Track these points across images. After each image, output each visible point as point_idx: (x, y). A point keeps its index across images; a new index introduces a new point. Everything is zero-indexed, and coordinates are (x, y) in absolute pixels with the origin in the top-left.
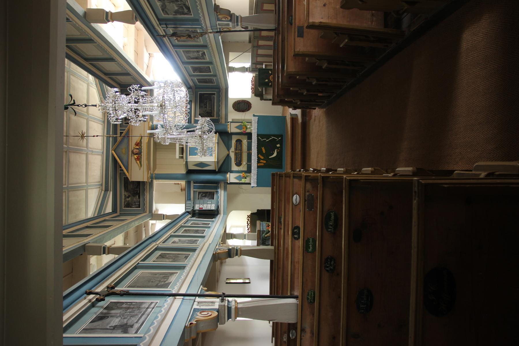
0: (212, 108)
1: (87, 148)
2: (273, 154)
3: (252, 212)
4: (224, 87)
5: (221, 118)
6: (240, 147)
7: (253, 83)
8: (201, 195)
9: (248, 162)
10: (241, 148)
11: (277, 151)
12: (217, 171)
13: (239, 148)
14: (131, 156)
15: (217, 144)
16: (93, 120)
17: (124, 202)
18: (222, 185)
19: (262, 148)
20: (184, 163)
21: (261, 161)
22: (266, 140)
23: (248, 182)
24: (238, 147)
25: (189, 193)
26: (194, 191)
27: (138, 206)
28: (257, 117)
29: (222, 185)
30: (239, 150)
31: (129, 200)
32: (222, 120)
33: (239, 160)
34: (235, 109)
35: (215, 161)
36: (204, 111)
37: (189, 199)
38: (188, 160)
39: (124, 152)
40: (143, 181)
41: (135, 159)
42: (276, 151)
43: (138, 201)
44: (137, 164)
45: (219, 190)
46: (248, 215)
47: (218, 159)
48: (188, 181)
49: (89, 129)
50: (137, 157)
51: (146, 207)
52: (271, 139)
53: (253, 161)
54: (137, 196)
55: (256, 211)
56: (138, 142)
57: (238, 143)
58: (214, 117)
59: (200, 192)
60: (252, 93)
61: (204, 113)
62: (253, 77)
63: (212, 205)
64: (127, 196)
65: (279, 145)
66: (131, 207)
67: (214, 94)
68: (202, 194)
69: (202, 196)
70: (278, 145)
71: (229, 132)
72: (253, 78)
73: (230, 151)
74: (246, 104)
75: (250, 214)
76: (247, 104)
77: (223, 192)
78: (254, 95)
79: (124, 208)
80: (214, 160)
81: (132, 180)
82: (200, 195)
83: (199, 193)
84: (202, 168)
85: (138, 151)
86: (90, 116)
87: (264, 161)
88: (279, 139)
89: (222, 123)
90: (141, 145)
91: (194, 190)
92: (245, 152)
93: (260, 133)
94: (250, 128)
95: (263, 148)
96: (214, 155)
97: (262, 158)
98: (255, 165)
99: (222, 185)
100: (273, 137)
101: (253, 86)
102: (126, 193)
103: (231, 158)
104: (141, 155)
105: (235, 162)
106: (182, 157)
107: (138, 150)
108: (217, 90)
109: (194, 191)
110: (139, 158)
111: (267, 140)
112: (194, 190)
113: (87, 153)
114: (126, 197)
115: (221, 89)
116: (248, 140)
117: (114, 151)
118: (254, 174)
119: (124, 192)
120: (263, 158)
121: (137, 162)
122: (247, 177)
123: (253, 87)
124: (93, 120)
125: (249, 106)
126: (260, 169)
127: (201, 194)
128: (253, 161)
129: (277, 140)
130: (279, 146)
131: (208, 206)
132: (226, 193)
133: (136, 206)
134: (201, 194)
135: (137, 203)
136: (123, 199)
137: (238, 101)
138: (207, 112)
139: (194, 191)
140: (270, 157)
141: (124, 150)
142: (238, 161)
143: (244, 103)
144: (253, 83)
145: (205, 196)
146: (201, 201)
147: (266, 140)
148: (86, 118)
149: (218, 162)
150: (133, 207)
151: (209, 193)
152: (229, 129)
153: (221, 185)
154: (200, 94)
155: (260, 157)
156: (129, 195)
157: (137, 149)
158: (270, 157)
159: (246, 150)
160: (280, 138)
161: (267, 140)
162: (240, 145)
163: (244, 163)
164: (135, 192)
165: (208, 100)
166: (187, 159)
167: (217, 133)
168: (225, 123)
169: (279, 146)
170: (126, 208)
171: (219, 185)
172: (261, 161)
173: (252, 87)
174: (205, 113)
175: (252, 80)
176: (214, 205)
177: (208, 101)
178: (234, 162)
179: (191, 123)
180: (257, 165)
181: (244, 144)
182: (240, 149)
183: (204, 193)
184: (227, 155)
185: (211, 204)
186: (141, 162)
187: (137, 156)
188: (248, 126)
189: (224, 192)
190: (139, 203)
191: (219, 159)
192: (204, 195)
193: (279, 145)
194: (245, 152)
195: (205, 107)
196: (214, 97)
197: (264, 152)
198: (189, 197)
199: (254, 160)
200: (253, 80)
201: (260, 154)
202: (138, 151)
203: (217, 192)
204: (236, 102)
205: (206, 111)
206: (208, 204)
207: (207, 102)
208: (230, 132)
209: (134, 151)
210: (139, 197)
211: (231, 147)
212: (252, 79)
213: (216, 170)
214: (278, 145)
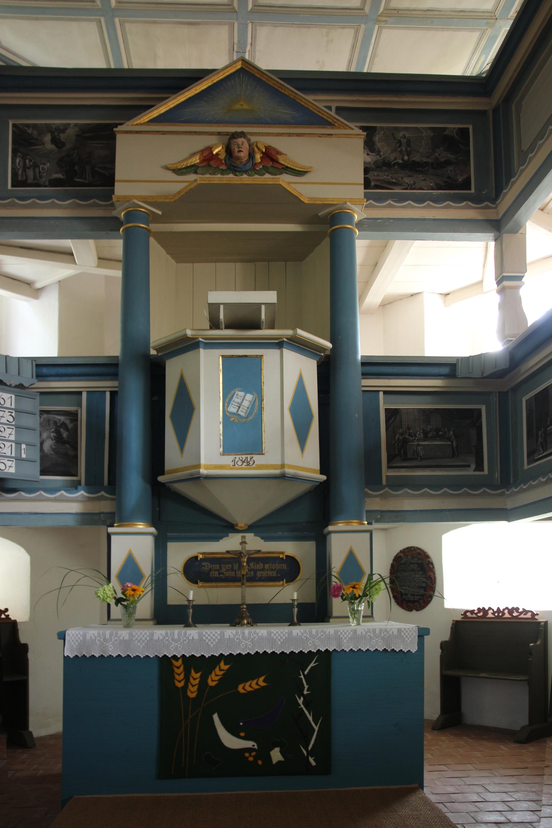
0: (422, 459)
1: (252, 11)
2: (234, 731)
3: (19, 627)
4: (510, 504)
5: (384, 497)
6: (264, 574)
7: (507, 615)
8: (64, 425)
9: (195, 607)
10: (261, 580)
11: (249, 750)
12: (161, 479)
13: (263, 569)
14: (219, 134)
15: (277, 472)
16: (357, 50)
17: (35, 126)
18: (105, 506)
19: (262, 679)
20: (189, 333)
21: (198, 675)
22: (301, 694)
23: (113, 616)
24: (267, 566)
25: (70, 370)
26: (80, 393)
27: (20, 178)
28: (414, 649)
29: (105, 506)
30: (255, 571)
31: (44, 144)
32: (378, 500)
33: (210, 570)
34: (402, 555)
35: (199, 466)
36: (409, 429)
37: (45, 371)
38: (201, 350)
39: (237, 107)
40: (116, 179)
41: (210, 149)
42: (249, 744)
43: (41, 177)
44: (186, 155)
45: (82, 493)
46: (7, 610)
47: (208, 478)
48: (116, 365)
49: (325, 30)
50: (217, 154)
51: (12, 206)
52: (310, 718)
53: (196, 637)
54: (60, 176)
55: (23, 639)
56: (279, 156)
57: (284, 566)
58: (389, 467)
59: (77, 420)
60: (467, 611)
61: (401, 431)
62: (533, 615)
63: (9, 463)
64: (63, 137)
65: (281, 758)
66: (15, 152)
67: (479, 466)
68: (70, 426)
69: (58, 427)
70: (276, 755)
71: (331, 528)
72: (529, 615)
73: (250, 537)
74: (422, 592)
75: (13, 617)
76: (422, 595)
77: (75, 508)
78: (459, 618)
79: (14, 125)
80: (203, 462)
81: (119, 137)
82: (62, 418)
83: (74, 416)
84: (172, 416)
85: (242, 154)
86: (373, 29)
87: (195, 688)
88: (311, 760)
89: (366, 499)
90: (266, 170)
91: (84, 395)
92: (243, 597)
93: (336, 664)
94: (355, 612)
95: (261, 682)
96: (228, 460)
97: (213, 680)
98: (174, 644)
99: (103, 503)
100: (316, 728)
101: (494, 613)
102: (71, 132)
103: (217, 539)
104: (223, 172)
105: (201, 556)
106: (215, 324)
107: (244, 155)
108: (497, 475)
109: (75, 397)
110: (212, 163)
111: (301, 701)
112: (84, 395)
113: (234, 11)
114: (56, 134)
115: (502, 494)
116: (300, 605)
117: (242, 69)
118: (126, 643)
119: (76, 125)
120: (211, 684)
121: (194, 154)
122: (125, 607)
123: (490, 615)
124: (357, 50)
125: (414, 602)
126: (154, 671)
127: (68, 422)
128: (196, 637)
129: (306, 748)
130: (275, 761)
131: (8, 444)
132: (70, 522)
133: (20, 172)
134: (68, 422)
135: (30, 173)
136: (48, 122)
137: (432, 564)
138: (405, 442)
139: (80, 393)
140: (216, 717)
141: (245, 107)
142: (206, 569)
143: (424, 585)
144: (507, 615)
145: (59, 439)
146: (34, 421)
147: (301, 694)
148: (367, 9)
149: (196, 479)
150: (18, 161)
151: (71, 453)
152: (341, 526)
153: (106, 499)
154: (480, 411)
155: (214, 668)
156: (63, 144)
157: (251, 155)
158: (216, 717)
159: (249, 601)
160: (313, 763)
161: (301, 701)
162: (274, 574)
163: (191, 593)
164: (76, 168)
165: (455, 445)
166: (212, 344)
167: (324, 478)
168: (367, 512)
169: (275, 761)
170: (14, 132)
171: (103, 493)
172: (196, 676)
173: (491, 611)
174: (402, 434)
175: (517, 609)
176: (12, 470)
177: (452, 445)
178: (203, 554)
179: (365, 375)
180: (175, 657)
181: (279, 589)
182: (259, 574)
183: (74, 433)
184: (229, 520)
185: (18, 459)
186: (196, 173)
187: (222, 156)
188: (362, 607)
189: (77, 514)
190: (30, 181)
191: (209, 484)
192: (65, 434)
193: (281, 758)
194: (243, 597)
195: (425, 433)
196: (469, 466)
197: (240, 689)
198: (53, 371)
199: (201, 639)
200: (521, 613)
201: (227, 670)
202: (242, 154)
203: (75, 486)
204: (427, 557)
205: (410, 435)
206: (18, 444)
207: (449, 439)
208: (330, 533)
209: (240, 140)
210: (55, 183)
211: (266, 539)
212: (525, 612)
213: (162, 472)
214: (276, 755)
